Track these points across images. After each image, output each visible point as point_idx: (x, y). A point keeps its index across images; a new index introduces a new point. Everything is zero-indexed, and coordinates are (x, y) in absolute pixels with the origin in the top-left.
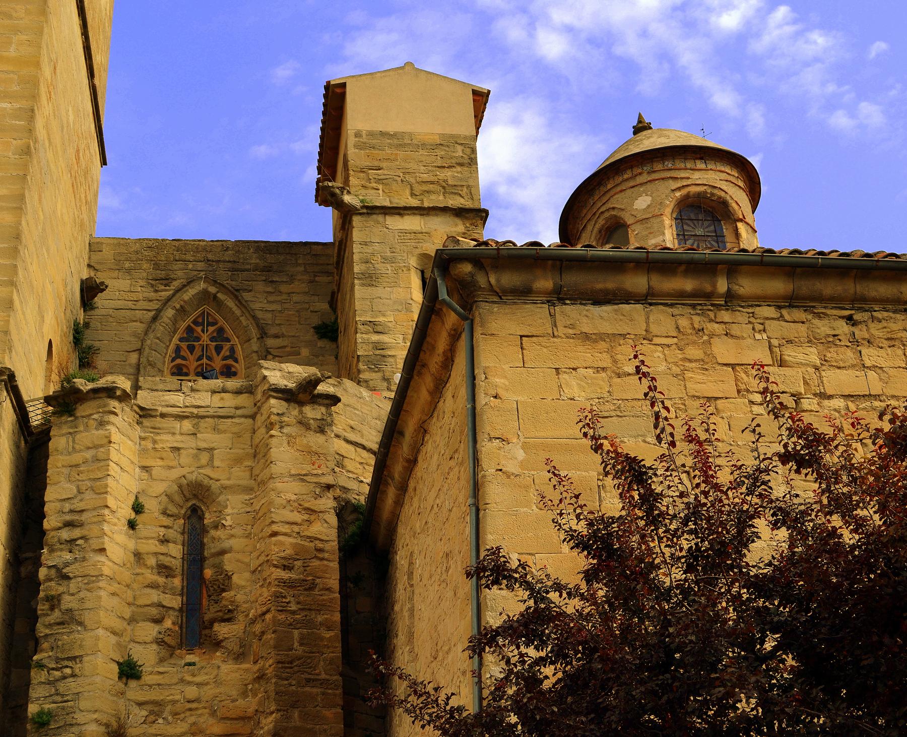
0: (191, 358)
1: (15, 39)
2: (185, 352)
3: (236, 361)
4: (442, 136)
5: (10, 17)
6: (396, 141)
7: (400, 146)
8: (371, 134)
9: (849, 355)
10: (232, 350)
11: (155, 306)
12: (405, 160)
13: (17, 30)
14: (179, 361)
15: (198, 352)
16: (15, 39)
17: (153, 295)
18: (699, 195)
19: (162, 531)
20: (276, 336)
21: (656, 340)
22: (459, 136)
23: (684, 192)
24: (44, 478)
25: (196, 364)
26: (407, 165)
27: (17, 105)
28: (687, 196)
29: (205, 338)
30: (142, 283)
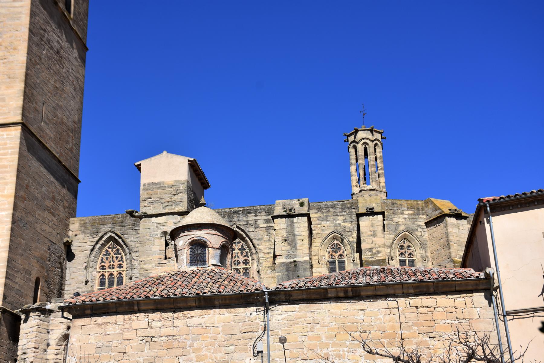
0: (107, 262)
1: (6, 187)
2: (105, 260)
3: (123, 262)
4: (175, 181)
5: (5, 179)
6: (158, 186)
7: (159, 188)
8: (149, 184)
9: (170, 323)
10: (122, 257)
11: (93, 244)
12: (160, 194)
13: (6, 184)
14: (103, 264)
15: (109, 259)
16: (6, 187)
17: (92, 240)
18: (196, 240)
19: (56, 351)
20: (136, 252)
21: (118, 323)
22: (181, 181)
23: (192, 240)
24: (19, 338)
25: (109, 264)
26: (161, 196)
27: (7, 213)
28: (193, 241)
29: (112, 254)
30: (88, 235)
